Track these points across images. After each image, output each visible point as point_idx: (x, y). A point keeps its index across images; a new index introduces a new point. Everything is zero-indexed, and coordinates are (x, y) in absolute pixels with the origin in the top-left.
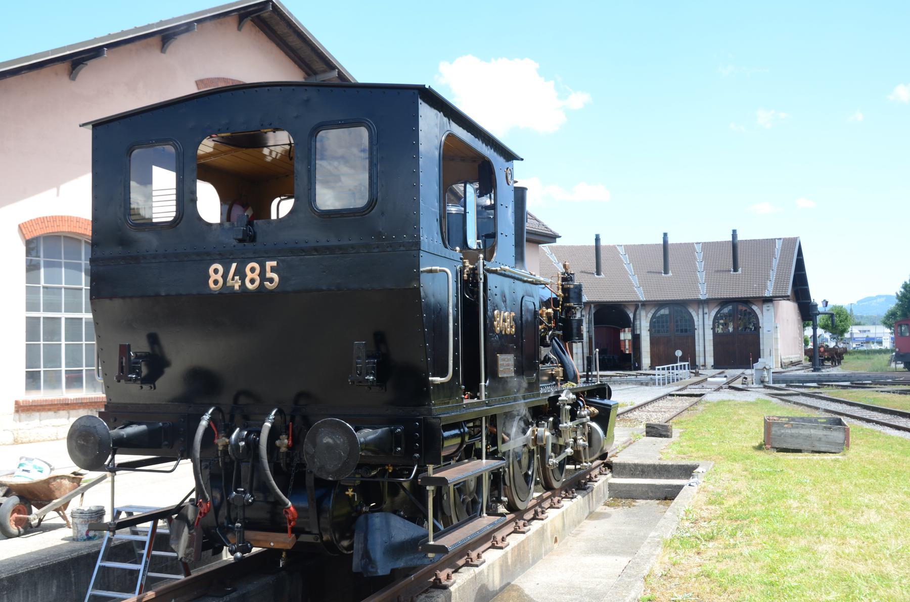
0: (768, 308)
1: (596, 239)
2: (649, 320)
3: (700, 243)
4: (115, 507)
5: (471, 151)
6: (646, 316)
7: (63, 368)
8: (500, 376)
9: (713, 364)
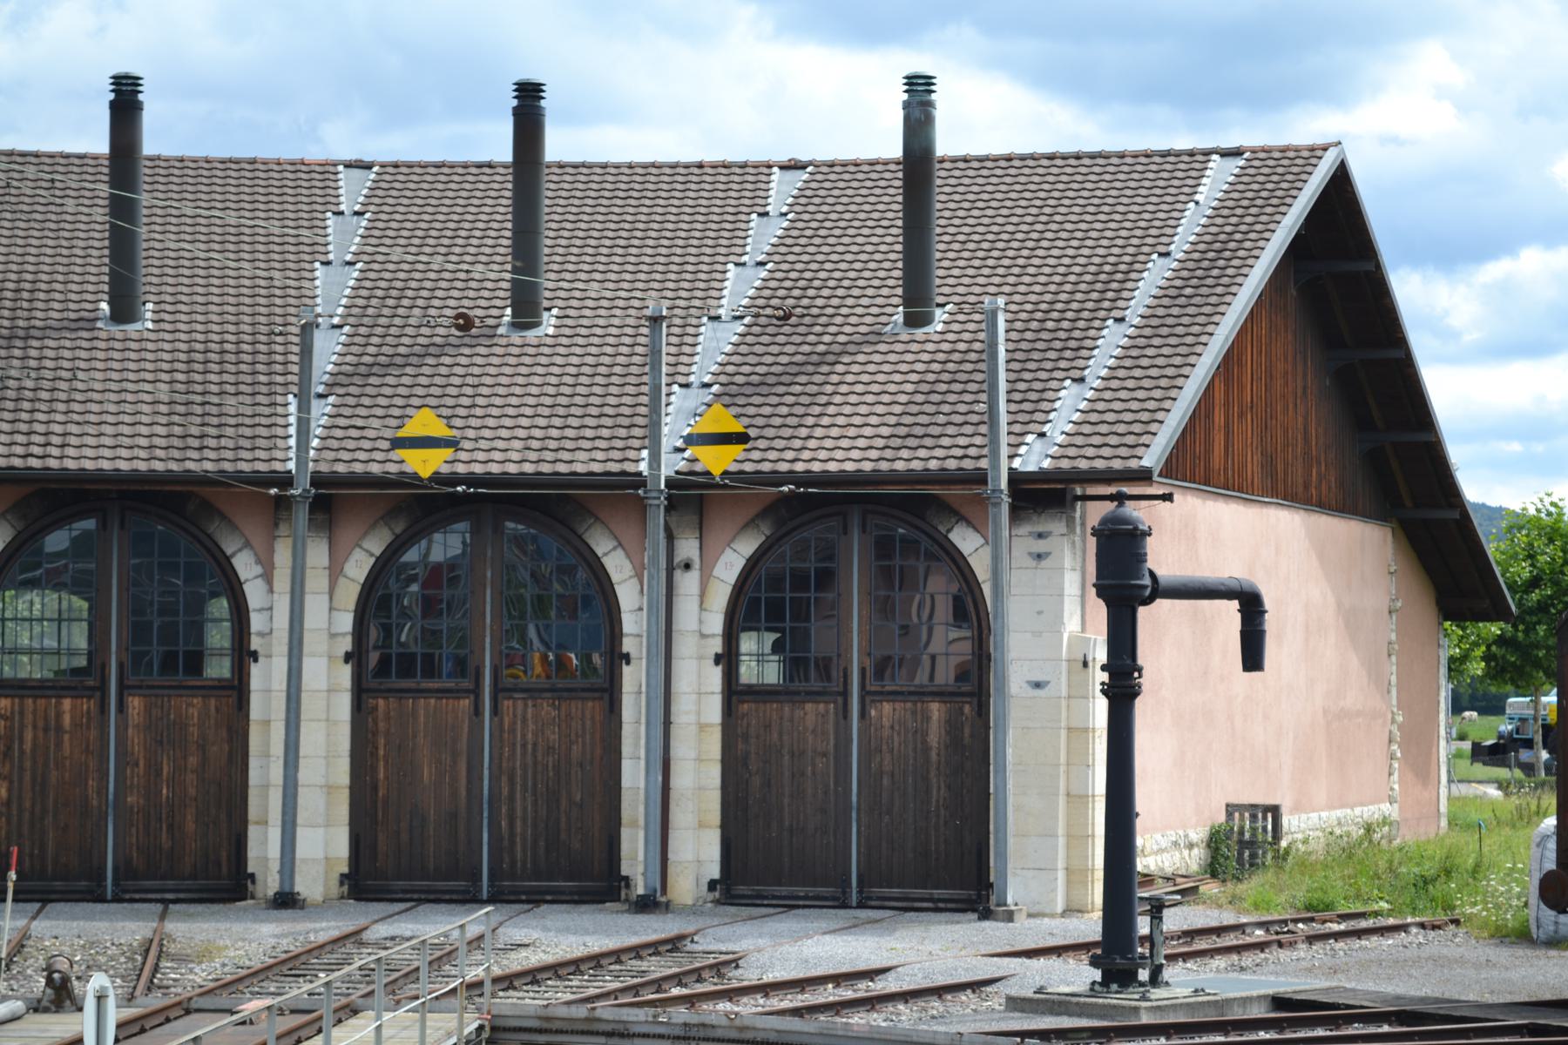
0: (1041, 546)
1: (114, 106)
2: (349, 593)
3: (368, 166)
5: (140, 687)
6: (335, 571)
9: (715, 872)
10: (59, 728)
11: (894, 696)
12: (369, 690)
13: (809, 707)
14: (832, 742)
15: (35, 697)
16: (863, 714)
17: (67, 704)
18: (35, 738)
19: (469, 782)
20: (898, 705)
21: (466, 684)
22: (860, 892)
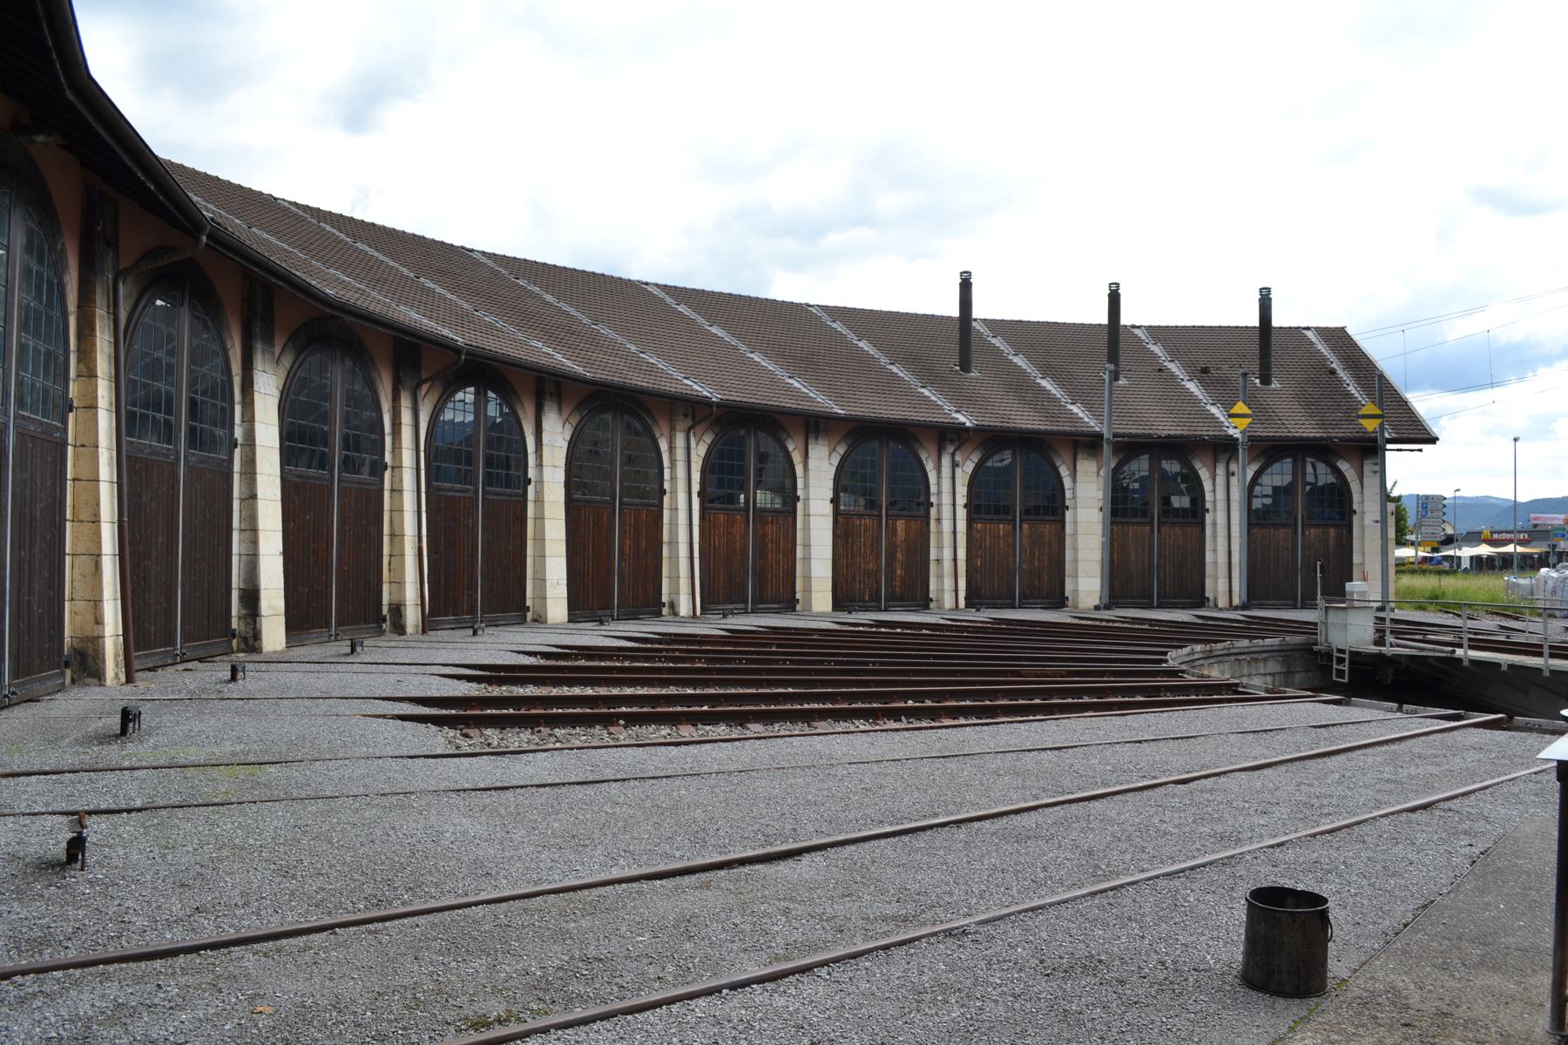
4: (1276, 322)
7: (735, 477)
8: (898, 523)
10: (999, 536)
11: (1315, 526)
12: (973, 519)
13: (1281, 530)
14: (1290, 544)
15: (991, 524)
16: (1303, 533)
17: (1001, 526)
18: (990, 541)
19: (1149, 558)
20: (1317, 530)
21: (1148, 520)
22: (1302, 602)
